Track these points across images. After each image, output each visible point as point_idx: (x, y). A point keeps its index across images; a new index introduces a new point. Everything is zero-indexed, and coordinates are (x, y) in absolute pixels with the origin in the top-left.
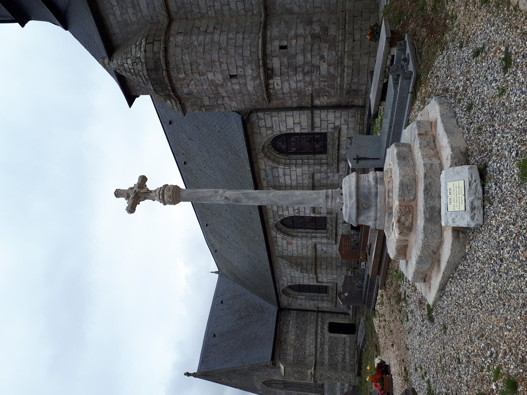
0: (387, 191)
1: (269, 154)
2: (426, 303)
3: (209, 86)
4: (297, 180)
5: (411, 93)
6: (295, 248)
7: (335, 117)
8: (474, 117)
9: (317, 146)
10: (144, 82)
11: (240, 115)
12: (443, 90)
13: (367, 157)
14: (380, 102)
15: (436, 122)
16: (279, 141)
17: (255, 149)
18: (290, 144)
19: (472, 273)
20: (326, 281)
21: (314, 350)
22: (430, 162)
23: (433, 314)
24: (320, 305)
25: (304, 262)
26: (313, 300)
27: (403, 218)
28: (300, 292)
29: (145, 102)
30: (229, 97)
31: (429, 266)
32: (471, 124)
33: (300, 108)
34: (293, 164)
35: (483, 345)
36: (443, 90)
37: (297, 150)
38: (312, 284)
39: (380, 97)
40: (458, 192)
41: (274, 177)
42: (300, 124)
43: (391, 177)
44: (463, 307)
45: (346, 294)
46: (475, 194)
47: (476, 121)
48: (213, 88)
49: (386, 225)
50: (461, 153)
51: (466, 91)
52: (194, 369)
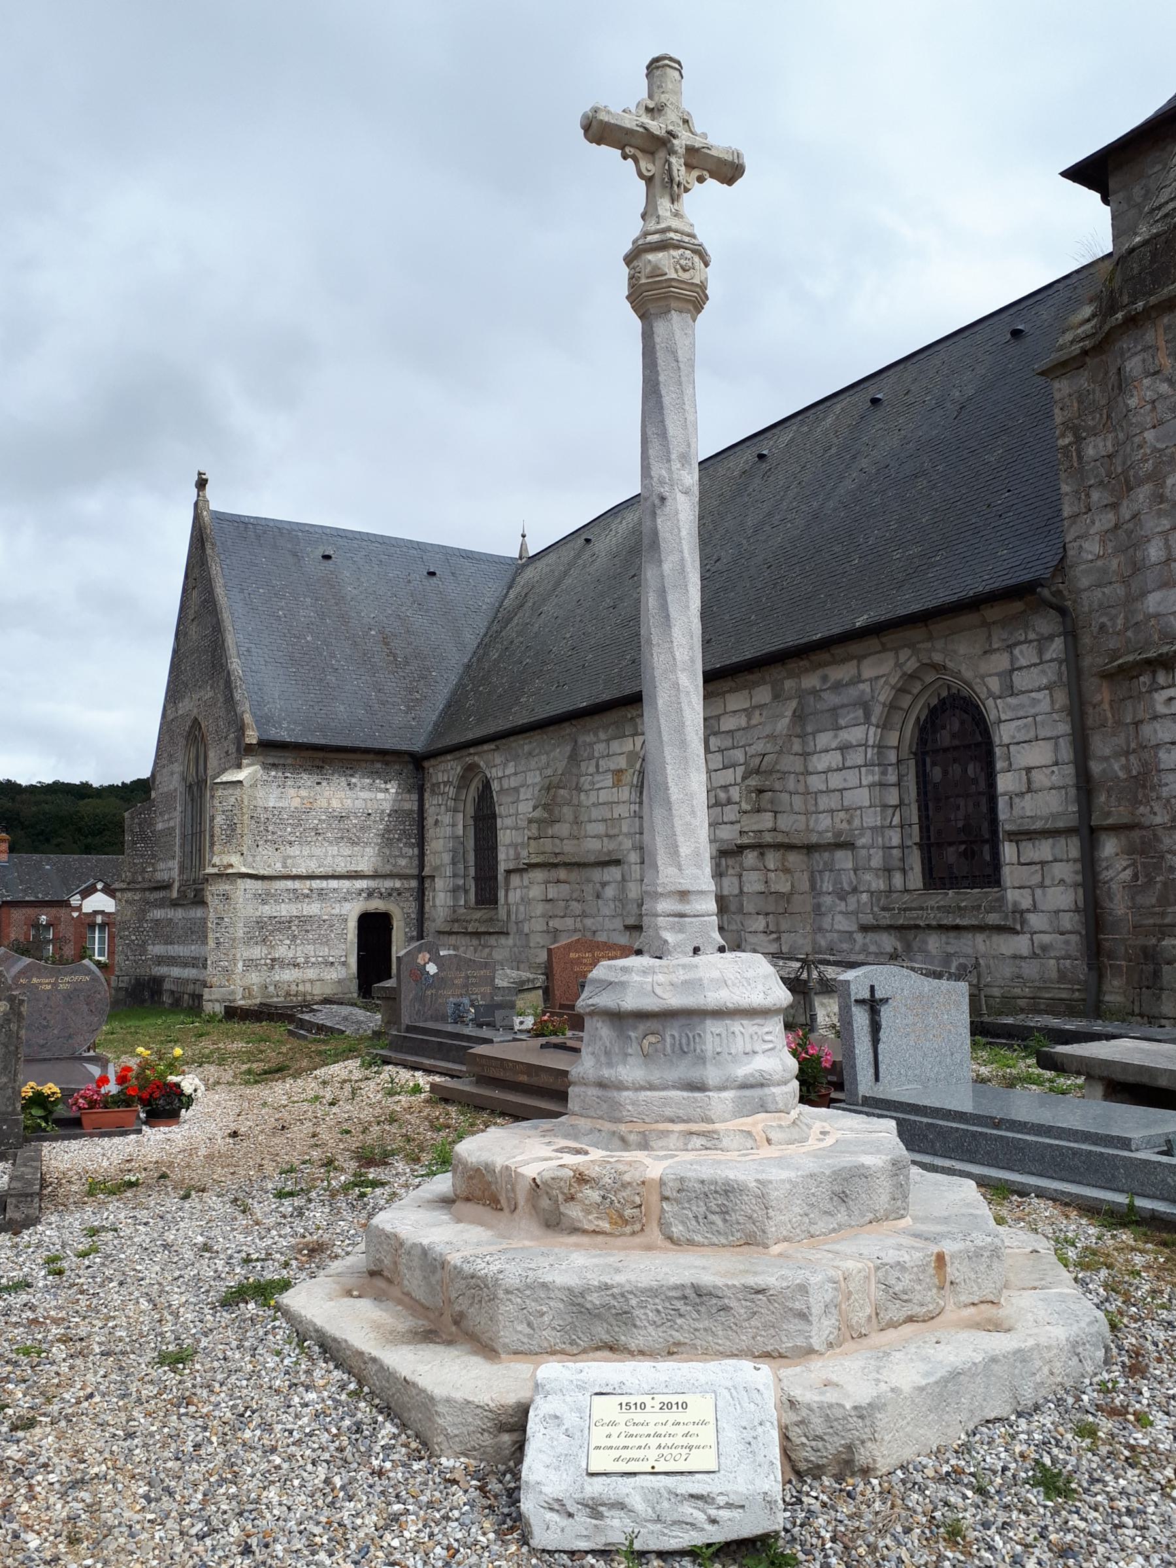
0: (710, 1127)
1: (917, 688)
2: (303, 1275)
3: (1155, 450)
4: (828, 791)
5: (1131, 1206)
6: (604, 796)
7: (1057, 912)
8: (1007, 1507)
9: (951, 854)
10: (1159, 208)
11: (1054, 575)
12: (1137, 1353)
13: (882, 1035)
14: (1101, 1079)
15: (996, 1326)
16: (962, 723)
17: (930, 638)
18: (955, 761)
19: (343, 1488)
20: (511, 899)
21: (302, 871)
22: (817, 1310)
23: (251, 1305)
24: (439, 883)
25: (563, 829)
26: (454, 863)
27: (594, 1195)
28: (476, 818)
29: (1085, 229)
30: (1117, 526)
31: (419, 1294)
32: (981, 1491)
33: (1085, 786)
34: (884, 773)
35: (33, 1545)
36: (1137, 1353)
37: (936, 785)
38: (501, 856)
39: (1121, 1077)
40: (669, 1441)
41: (834, 711)
42: (1029, 790)
43: (769, 1141)
44: (224, 1444)
45: (432, 969)
46: (659, 1520)
47: (989, 1513)
48: (1149, 466)
49: (583, 1123)
50: (850, 1448)
51: (1131, 1463)
52: (219, 501)
